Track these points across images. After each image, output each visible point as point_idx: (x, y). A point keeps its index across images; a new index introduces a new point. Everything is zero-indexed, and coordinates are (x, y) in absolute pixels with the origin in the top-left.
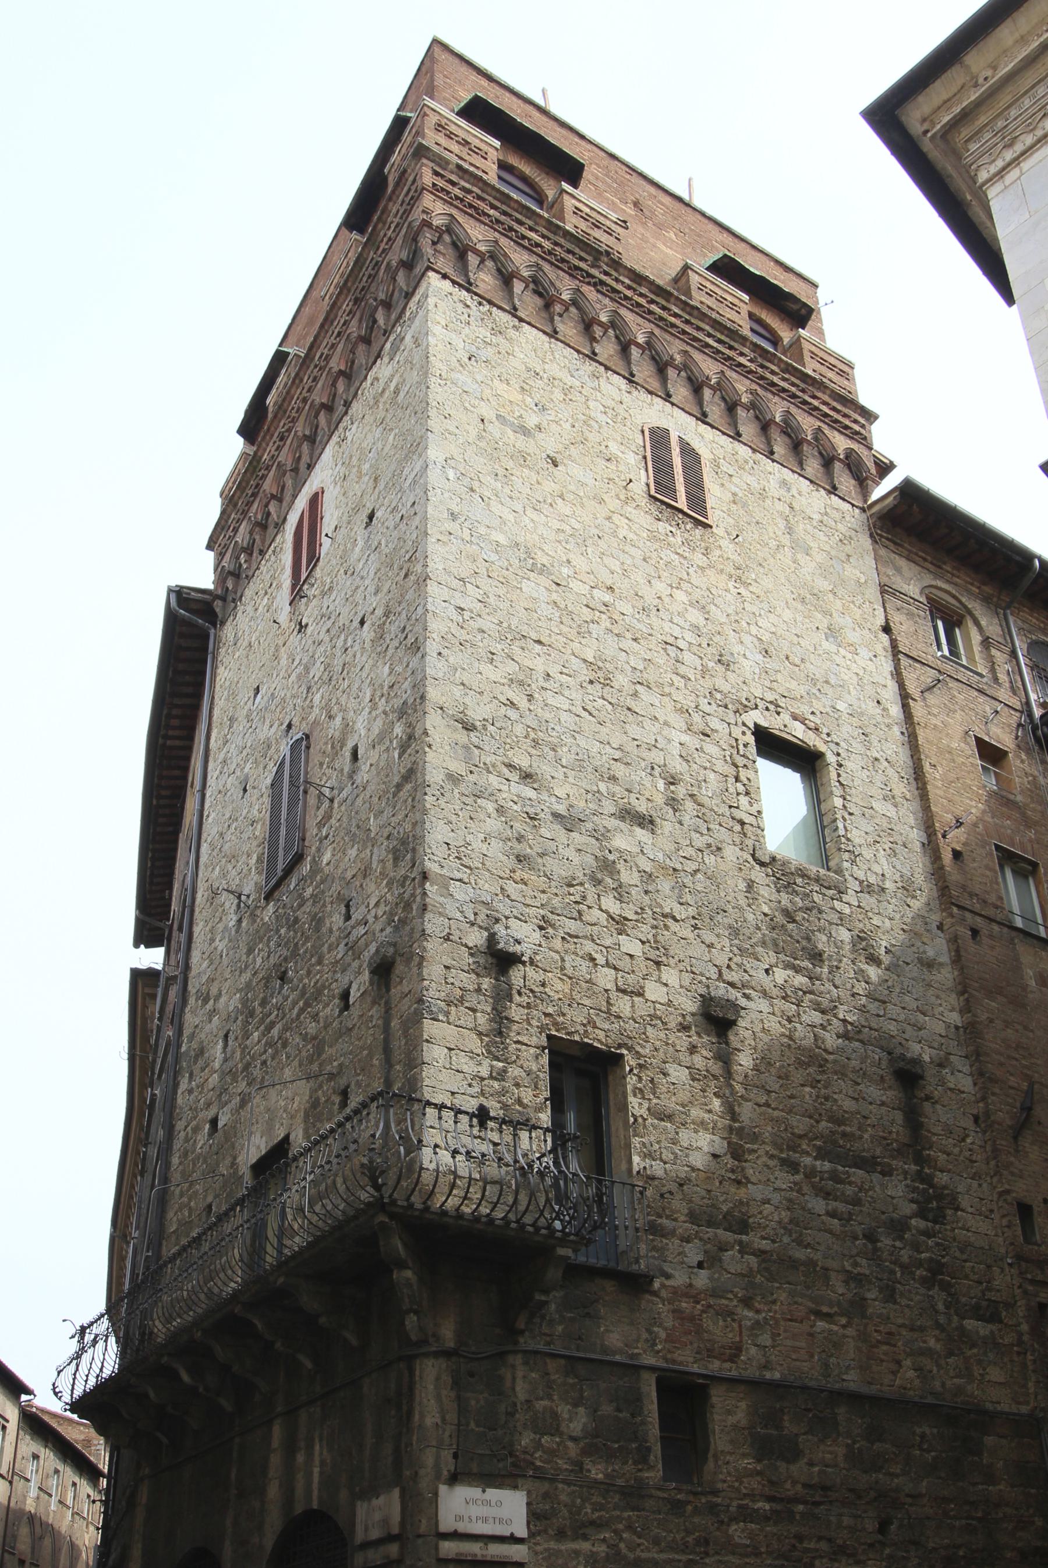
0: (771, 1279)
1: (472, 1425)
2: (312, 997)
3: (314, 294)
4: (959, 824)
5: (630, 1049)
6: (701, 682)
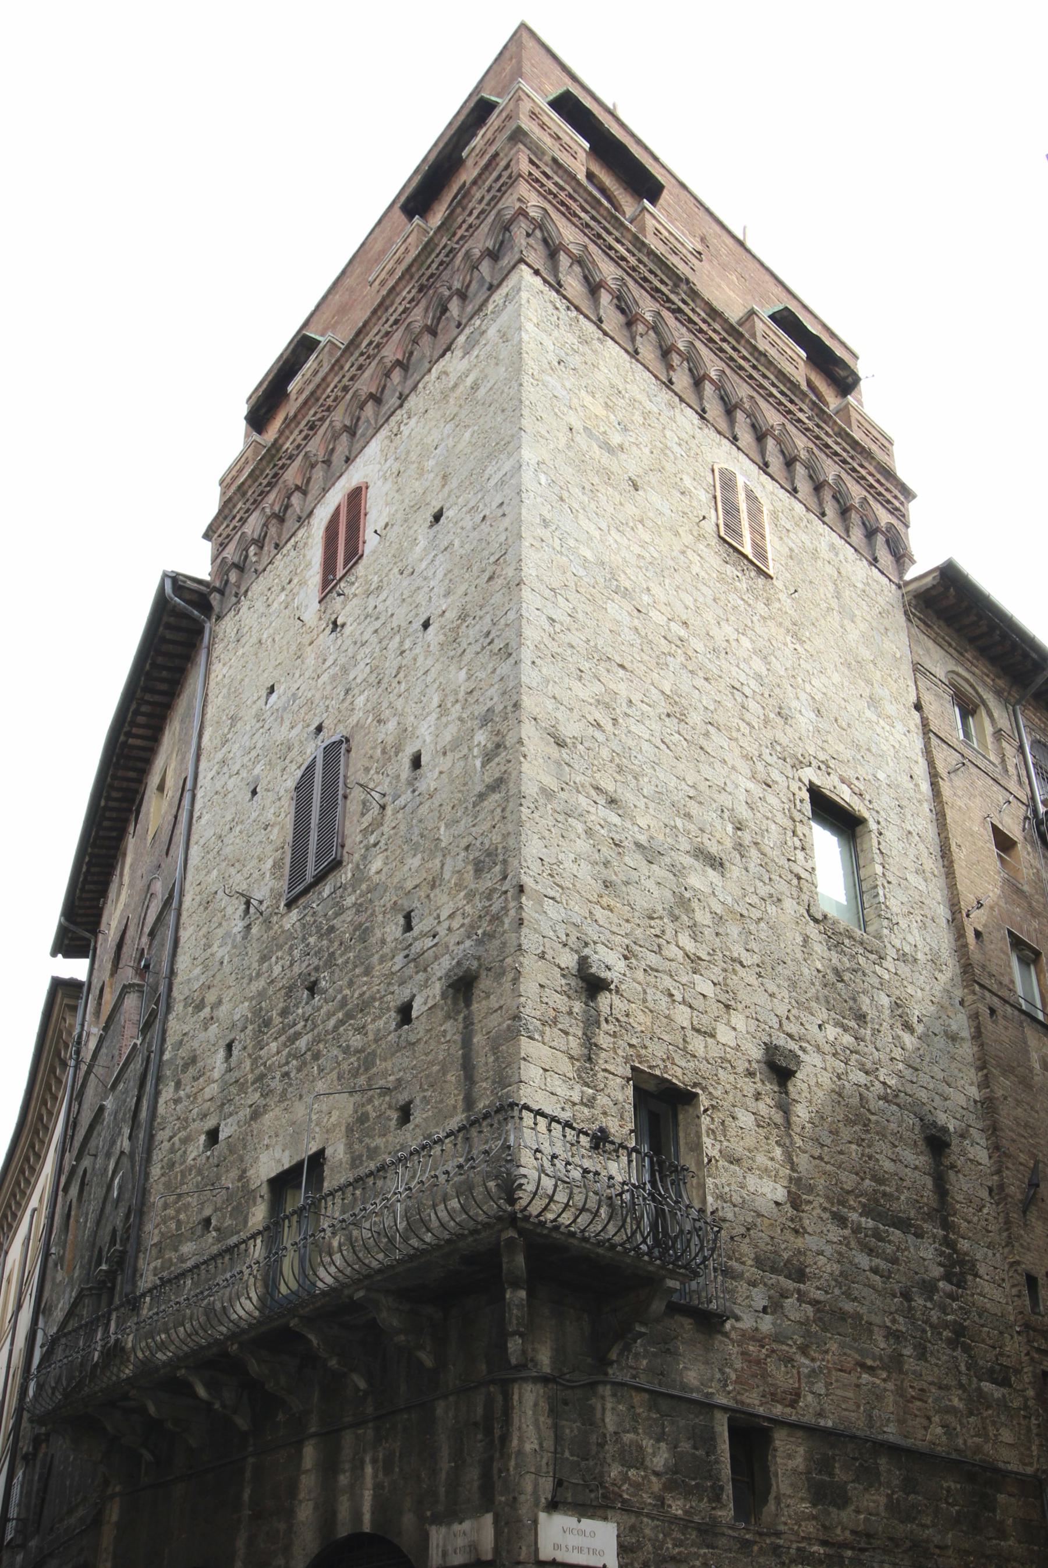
0: (825, 1329)
1: (567, 1454)
2: (354, 1012)
3: (348, 281)
4: (980, 905)
5: (704, 1089)
6: (764, 731)
